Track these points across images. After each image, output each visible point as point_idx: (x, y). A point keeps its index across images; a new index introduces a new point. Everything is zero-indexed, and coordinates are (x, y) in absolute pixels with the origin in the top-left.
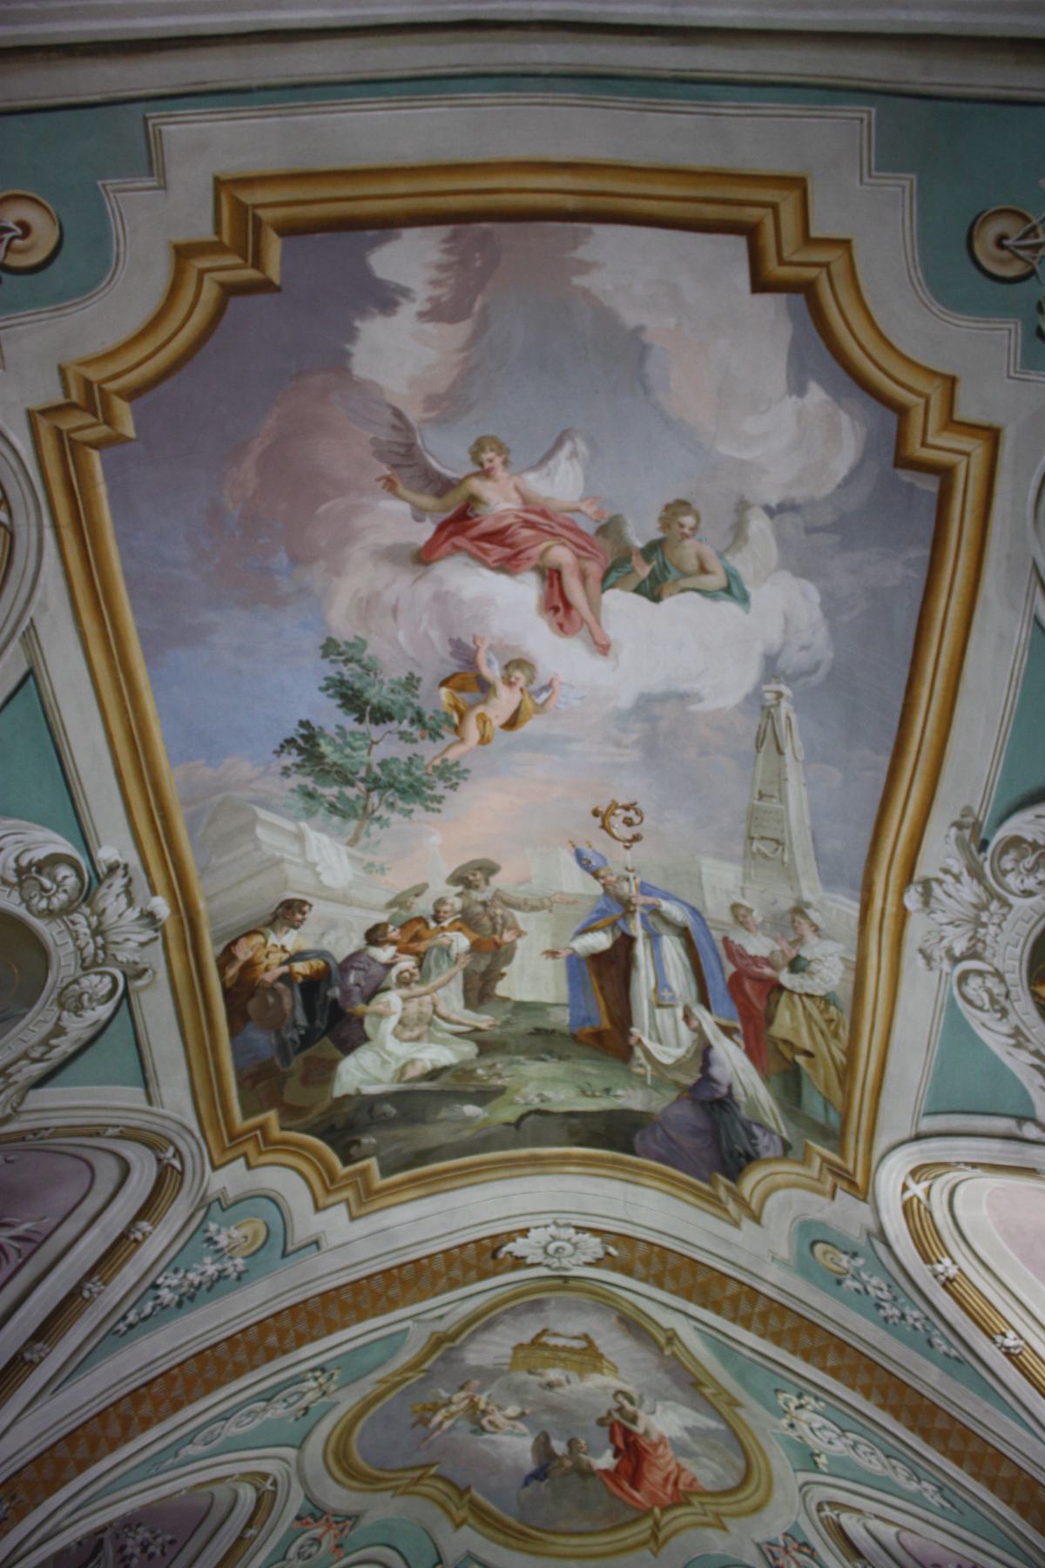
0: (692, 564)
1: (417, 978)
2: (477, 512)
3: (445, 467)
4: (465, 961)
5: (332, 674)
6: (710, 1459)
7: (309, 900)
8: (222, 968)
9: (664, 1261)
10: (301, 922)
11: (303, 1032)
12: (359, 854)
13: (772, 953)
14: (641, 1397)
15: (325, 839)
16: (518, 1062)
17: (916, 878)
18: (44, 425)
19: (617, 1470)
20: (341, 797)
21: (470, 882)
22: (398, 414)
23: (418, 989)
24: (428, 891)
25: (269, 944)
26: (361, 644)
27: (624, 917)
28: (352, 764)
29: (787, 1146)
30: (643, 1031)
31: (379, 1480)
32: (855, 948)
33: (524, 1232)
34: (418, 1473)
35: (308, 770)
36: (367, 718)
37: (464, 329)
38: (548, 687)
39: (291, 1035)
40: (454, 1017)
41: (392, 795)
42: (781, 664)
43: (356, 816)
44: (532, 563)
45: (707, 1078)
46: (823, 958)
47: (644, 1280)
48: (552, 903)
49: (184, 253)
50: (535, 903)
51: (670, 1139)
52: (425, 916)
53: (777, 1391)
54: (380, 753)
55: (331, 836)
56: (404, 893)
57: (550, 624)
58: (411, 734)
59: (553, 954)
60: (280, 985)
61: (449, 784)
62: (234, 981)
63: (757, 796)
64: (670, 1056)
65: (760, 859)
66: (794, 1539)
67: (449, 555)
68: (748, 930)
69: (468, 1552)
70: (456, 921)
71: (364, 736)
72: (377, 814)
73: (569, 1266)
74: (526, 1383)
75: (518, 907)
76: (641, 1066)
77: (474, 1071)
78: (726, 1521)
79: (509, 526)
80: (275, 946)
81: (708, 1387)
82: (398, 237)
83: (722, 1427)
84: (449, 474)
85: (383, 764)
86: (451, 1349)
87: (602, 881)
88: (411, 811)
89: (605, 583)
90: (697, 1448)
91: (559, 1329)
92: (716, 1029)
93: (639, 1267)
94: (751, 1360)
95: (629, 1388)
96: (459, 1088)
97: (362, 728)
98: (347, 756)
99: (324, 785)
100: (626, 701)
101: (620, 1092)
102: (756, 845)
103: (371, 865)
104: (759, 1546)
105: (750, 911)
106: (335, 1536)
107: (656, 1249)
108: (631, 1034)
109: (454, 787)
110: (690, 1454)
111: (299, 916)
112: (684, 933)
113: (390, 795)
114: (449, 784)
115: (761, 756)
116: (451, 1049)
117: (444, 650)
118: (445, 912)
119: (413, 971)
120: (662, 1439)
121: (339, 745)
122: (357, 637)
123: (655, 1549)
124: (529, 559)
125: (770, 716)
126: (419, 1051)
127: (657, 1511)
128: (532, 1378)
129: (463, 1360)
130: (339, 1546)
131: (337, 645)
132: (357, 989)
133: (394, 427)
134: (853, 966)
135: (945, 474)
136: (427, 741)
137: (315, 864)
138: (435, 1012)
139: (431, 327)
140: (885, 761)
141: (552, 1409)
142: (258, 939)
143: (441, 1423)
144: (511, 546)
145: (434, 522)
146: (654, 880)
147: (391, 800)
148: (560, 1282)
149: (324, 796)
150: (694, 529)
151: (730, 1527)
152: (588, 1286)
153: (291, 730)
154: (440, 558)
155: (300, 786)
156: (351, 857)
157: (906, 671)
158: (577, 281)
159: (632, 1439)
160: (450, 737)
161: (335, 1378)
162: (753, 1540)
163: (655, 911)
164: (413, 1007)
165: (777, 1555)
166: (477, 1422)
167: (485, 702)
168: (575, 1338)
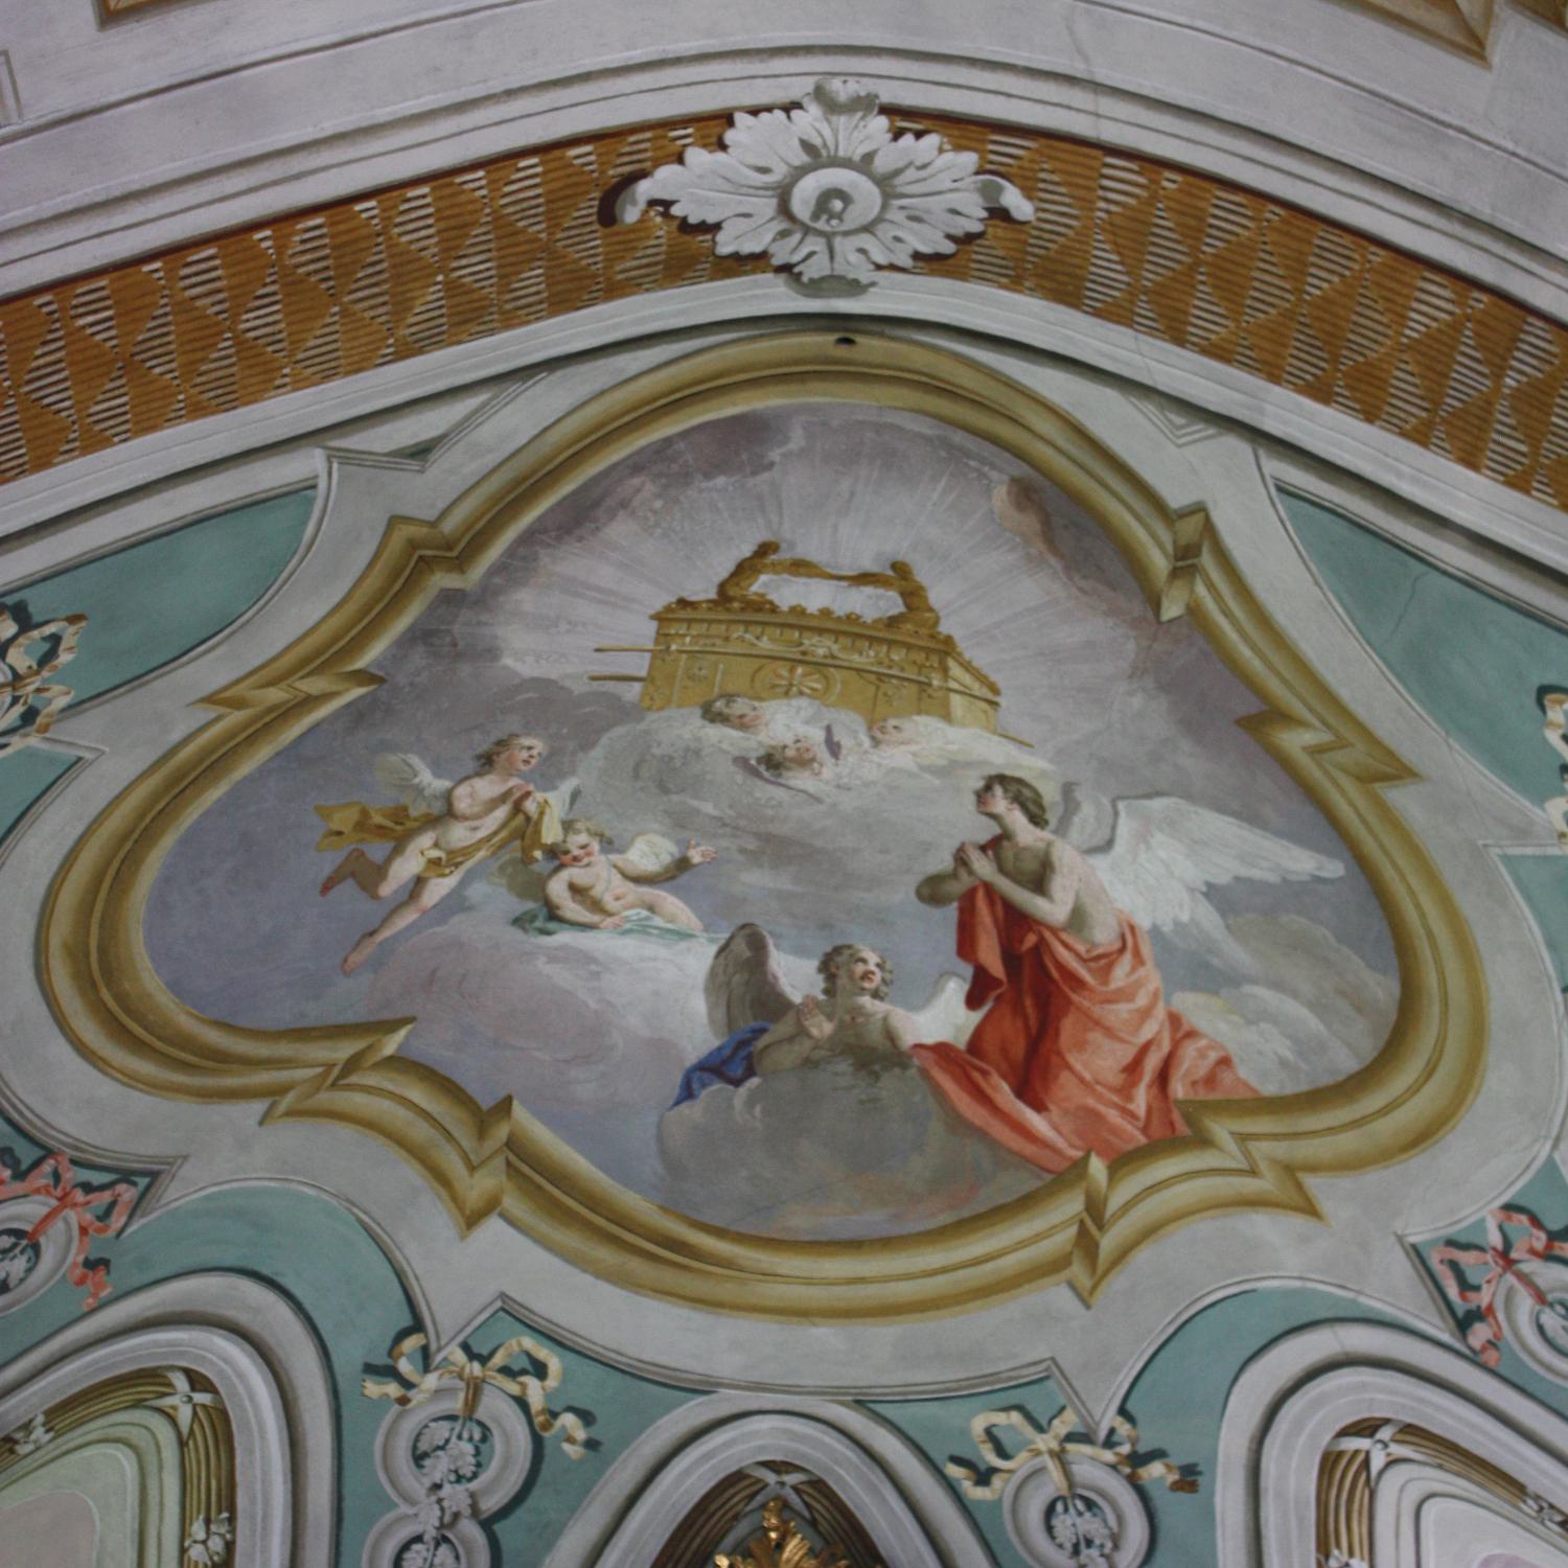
6: (1278, 985)
9: (1194, 229)
14: (1068, 790)
19: (975, 1045)
31: (222, 1059)
33: (714, 127)
34: (344, 1050)
47: (1116, 313)
53: (1543, 691)
66: (1535, 1221)
69: (503, 1296)
73: (865, 275)
74: (694, 752)
78: (1312, 1182)
81: (1301, 723)
83: (1334, 868)
86: (451, 599)
90: (1237, 954)
91: (810, 547)
93: (1105, 262)
94: (1470, 584)
95: (1029, 765)
104: (1417, 1253)
106: (83, 1231)
107: (1170, 182)
110: (1206, 974)
120: (1128, 938)
123: (1085, 1282)
127: (1097, 1167)
128: (714, 733)
129: (492, 653)
130: (95, 1265)
141: (775, 848)
143: (419, 882)
148: (822, 342)
151: (1325, 1205)
152: (917, 358)
159: (1031, 940)
161: (64, 658)
162: (1400, 1239)
165: (1473, 1277)
166: (535, 888)
168: (863, 579)
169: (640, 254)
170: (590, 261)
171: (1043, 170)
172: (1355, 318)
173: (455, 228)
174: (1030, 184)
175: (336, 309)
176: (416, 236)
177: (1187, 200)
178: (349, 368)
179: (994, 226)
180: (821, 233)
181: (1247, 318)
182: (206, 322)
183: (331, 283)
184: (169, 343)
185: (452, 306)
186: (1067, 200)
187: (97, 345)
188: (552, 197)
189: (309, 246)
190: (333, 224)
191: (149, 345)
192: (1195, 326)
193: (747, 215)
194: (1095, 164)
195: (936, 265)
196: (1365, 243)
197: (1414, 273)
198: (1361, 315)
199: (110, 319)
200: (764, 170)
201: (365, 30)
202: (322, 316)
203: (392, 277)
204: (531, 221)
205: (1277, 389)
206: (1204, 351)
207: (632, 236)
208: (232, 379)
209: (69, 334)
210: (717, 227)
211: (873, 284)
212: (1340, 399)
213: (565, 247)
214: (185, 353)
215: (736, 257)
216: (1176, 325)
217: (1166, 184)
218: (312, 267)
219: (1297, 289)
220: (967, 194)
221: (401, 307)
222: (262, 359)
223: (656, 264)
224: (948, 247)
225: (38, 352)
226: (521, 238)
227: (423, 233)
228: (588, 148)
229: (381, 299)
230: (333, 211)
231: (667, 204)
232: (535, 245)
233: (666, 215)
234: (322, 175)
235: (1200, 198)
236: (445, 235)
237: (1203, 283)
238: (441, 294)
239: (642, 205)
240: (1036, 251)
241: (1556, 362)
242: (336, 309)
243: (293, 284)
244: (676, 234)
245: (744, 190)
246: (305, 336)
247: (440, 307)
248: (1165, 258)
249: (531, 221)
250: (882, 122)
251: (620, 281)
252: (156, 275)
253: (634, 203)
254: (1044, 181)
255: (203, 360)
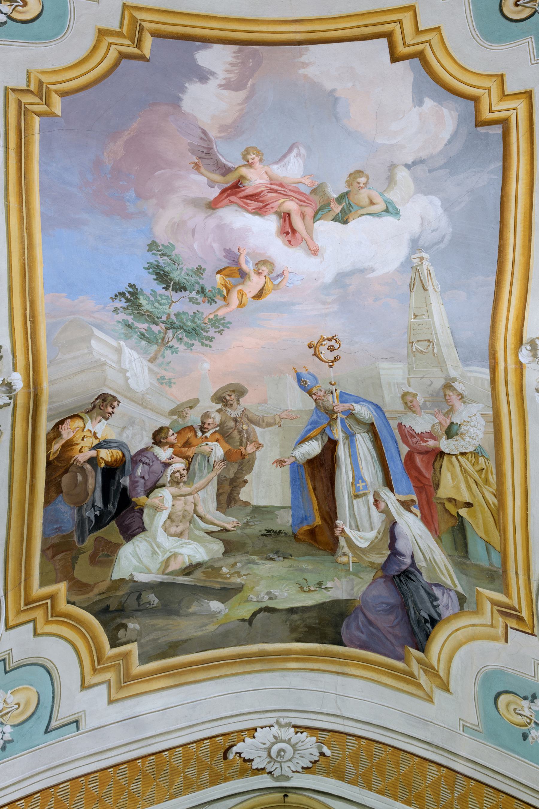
0: (366, 201)
1: (185, 479)
2: (244, 184)
3: (228, 161)
4: (219, 468)
5: (153, 261)
7: (119, 397)
8: (49, 442)
10: (110, 414)
11: (98, 513)
12: (156, 369)
13: (433, 426)
15: (135, 355)
16: (254, 563)
17: (524, 341)
18: (12, 97)
20: (149, 330)
21: (227, 401)
22: (204, 132)
23: (185, 489)
24: (198, 405)
25: (86, 429)
26: (172, 247)
27: (329, 425)
28: (159, 313)
29: (462, 599)
30: (345, 523)
32: (490, 404)
35: (130, 312)
36: (171, 288)
37: (242, 94)
38: (282, 275)
39: (90, 514)
40: (209, 517)
41: (181, 333)
42: (421, 242)
43: (157, 343)
44: (274, 210)
45: (394, 553)
46: (469, 420)
48: (281, 419)
49: (102, 33)
50: (271, 420)
51: (370, 623)
52: (195, 426)
54: (175, 308)
55: (139, 353)
56: (182, 404)
57: (283, 242)
58: (197, 299)
59: (280, 463)
60: (88, 467)
61: (217, 330)
62: (56, 455)
63: (413, 317)
64: (366, 540)
65: (418, 355)
67: (227, 205)
68: (414, 412)
70: (215, 432)
71: (167, 298)
72: (170, 344)
73: (290, 774)
75: (258, 424)
76: (345, 554)
77: (220, 568)
79: (262, 192)
80: (90, 431)
82: (211, 47)
84: (230, 164)
85: (177, 315)
87: (314, 397)
88: (193, 345)
89: (316, 217)
92: (398, 504)
96: (208, 584)
97: (167, 293)
98: (155, 307)
99: (139, 321)
100: (328, 278)
101: (329, 584)
102: (415, 345)
103: (163, 378)
105: (415, 395)
108: (336, 527)
109: (221, 332)
111: (110, 410)
112: (371, 428)
113: (180, 333)
114: (217, 330)
115: (413, 294)
116: (205, 547)
117: (220, 254)
118: (209, 424)
119: (182, 472)
121: (152, 301)
122: (169, 243)
124: (272, 208)
125: (417, 271)
126: (181, 546)
131: (157, 246)
132: (142, 481)
133: (201, 138)
134: (492, 419)
135: (505, 123)
136: (206, 304)
137: (126, 371)
138: (195, 511)
139: (225, 93)
140: (492, 279)
142: (79, 423)
144: (262, 202)
145: (219, 188)
146: (350, 390)
147: (180, 336)
149: (138, 328)
150: (366, 184)
153: (124, 287)
154: (222, 207)
155: (123, 320)
156: (150, 370)
157: (498, 227)
158: (301, 71)
160: (220, 302)
163: (350, 414)
164: (180, 504)
167: (243, 283)
169: (233, 768)
170: (220, 770)
171: (332, 741)
172: (413, 778)
173: (187, 760)
174: (329, 745)
175: (155, 784)
176: (177, 762)
177: (367, 747)
178: (157, 802)
179: (321, 758)
180: (278, 762)
181: (387, 781)
182: (122, 787)
183: (155, 776)
184: (111, 793)
185: (185, 783)
186: (338, 749)
187: (93, 793)
188: (212, 751)
189: (150, 765)
190: (157, 758)
191: (106, 793)
192: (374, 785)
193: (260, 757)
194: (345, 739)
195: (308, 770)
196: (413, 756)
197: (426, 764)
198: (415, 778)
199: (98, 785)
200: (264, 744)
201: (170, 706)
202: (151, 786)
203: (170, 774)
204: (206, 758)
205: (397, 802)
206: (377, 793)
207: (231, 763)
208: (126, 805)
209: (87, 790)
210: (253, 760)
211: (292, 777)
212: (414, 804)
213: (214, 766)
214: (115, 796)
215: (257, 769)
216: (369, 785)
217: (362, 743)
218: (150, 771)
219: (398, 771)
220: (314, 749)
221: (172, 783)
222: (134, 799)
223: (237, 771)
224: (310, 765)
225: (78, 795)
226: (203, 763)
227: (179, 761)
228: (221, 738)
229: (167, 781)
230: (157, 755)
231: (240, 754)
232: (207, 765)
233: (240, 757)
234: (155, 745)
235: (371, 747)
236: (185, 762)
237: (374, 771)
238: (182, 780)
239: (234, 754)
240: (332, 765)
241: (466, 787)
242: (155, 784)
243: (145, 776)
244: (242, 762)
245: (259, 750)
246: (146, 791)
247: (182, 784)
248: (364, 764)
249: (206, 758)
250: (293, 730)
251: (228, 777)
252: (111, 773)
253: (232, 753)
254: (332, 744)
255: (119, 799)
